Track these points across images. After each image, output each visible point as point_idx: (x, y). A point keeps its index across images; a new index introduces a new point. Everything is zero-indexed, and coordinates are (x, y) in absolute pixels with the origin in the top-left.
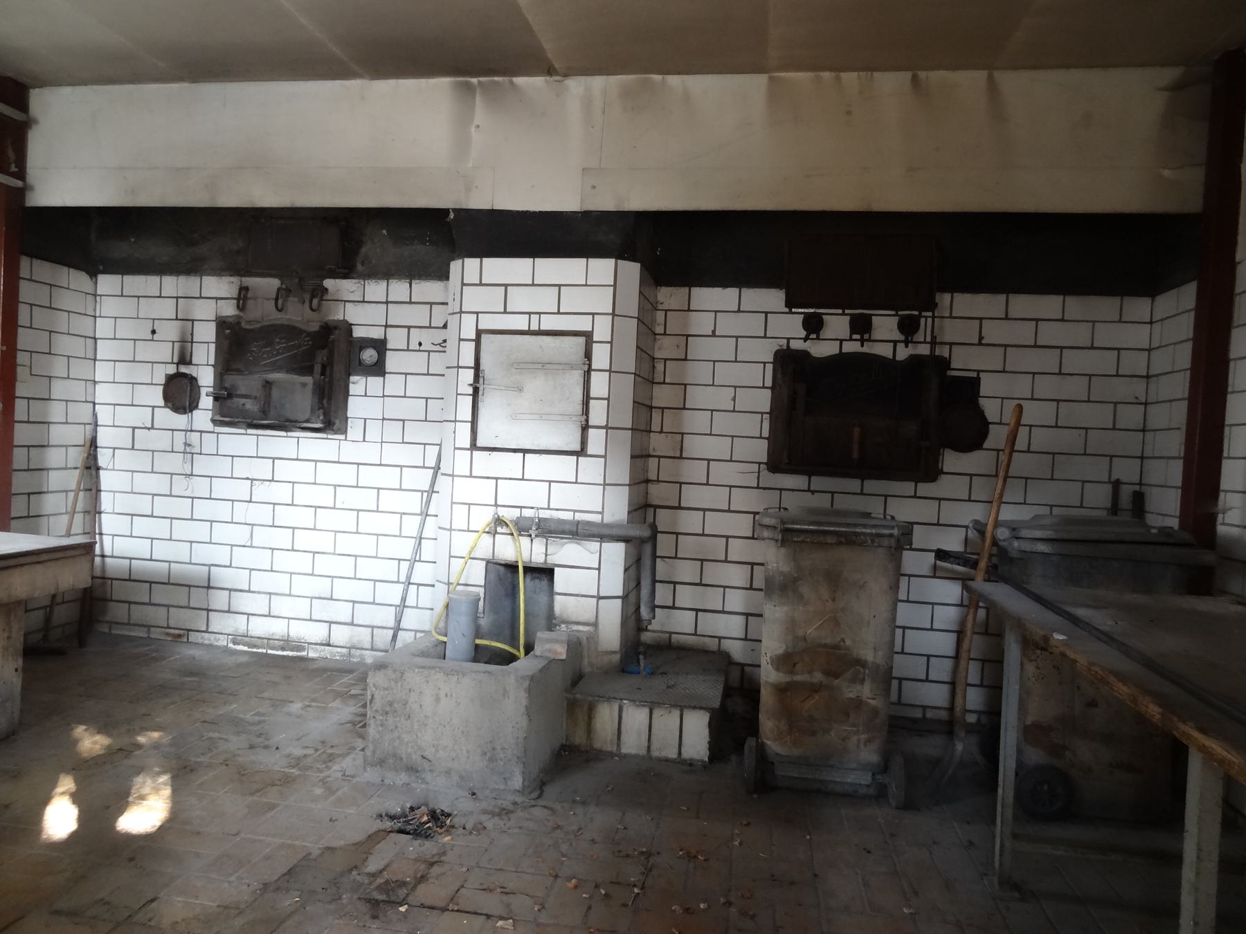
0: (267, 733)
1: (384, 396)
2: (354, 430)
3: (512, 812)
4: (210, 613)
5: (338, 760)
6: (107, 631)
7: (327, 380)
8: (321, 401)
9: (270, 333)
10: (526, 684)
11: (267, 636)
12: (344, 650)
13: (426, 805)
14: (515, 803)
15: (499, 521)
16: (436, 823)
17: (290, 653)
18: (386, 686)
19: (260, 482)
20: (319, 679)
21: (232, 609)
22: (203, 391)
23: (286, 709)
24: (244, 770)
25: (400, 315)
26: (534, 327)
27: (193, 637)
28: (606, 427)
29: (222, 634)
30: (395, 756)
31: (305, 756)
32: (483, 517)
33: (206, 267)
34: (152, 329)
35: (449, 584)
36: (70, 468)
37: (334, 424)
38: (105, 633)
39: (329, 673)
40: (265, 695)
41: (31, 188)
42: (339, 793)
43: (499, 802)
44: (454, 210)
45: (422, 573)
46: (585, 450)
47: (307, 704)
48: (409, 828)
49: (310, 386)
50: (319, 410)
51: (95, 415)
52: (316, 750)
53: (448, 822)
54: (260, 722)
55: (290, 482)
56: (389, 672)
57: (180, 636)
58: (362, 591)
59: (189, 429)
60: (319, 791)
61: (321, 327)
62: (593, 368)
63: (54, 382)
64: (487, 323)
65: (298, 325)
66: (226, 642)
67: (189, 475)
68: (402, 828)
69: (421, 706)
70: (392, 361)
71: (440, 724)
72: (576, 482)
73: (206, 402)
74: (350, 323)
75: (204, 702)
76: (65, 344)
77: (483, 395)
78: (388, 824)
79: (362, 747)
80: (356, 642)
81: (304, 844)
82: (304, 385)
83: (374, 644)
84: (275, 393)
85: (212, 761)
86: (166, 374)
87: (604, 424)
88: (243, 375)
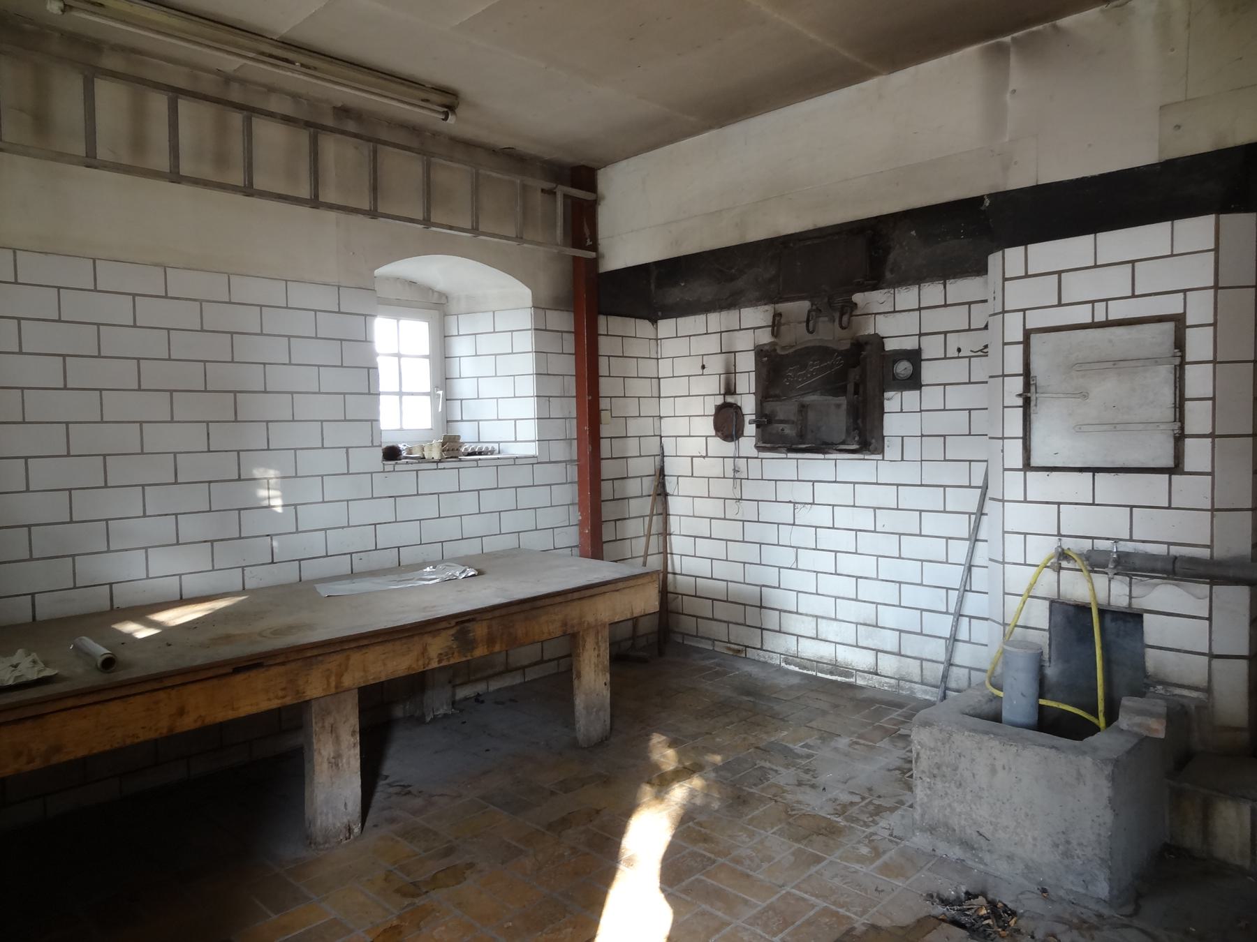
0: (815, 770)
1: (921, 411)
2: (891, 450)
3: (1097, 928)
4: (764, 632)
5: (884, 814)
6: (681, 641)
7: (860, 398)
8: (856, 418)
9: (803, 355)
10: (1108, 770)
11: (815, 659)
12: (893, 681)
13: (984, 895)
14: (1100, 916)
15: (1063, 555)
16: (997, 921)
17: (839, 679)
18: (932, 746)
19: (802, 506)
20: (867, 711)
21: (783, 630)
22: (747, 419)
23: (833, 744)
24: (792, 810)
25: (934, 321)
26: (1100, 317)
27: (751, 654)
28: (1212, 436)
29: (775, 653)
30: (946, 825)
31: (852, 804)
32: (1042, 549)
33: (743, 299)
34: (701, 364)
35: (1004, 625)
36: (645, 496)
37: (870, 444)
38: (679, 643)
39: (878, 705)
40: (814, 724)
41: (603, 256)
42: (885, 858)
43: (1079, 910)
44: (990, 196)
45: (973, 604)
46: (1180, 466)
47: (855, 740)
48: (964, 919)
49: (844, 407)
50: (854, 430)
51: (662, 447)
52: (863, 798)
53: (1012, 923)
54: (809, 756)
55: (830, 505)
56: (935, 730)
57: (739, 651)
58: (909, 620)
59: (737, 456)
60: (864, 850)
61: (852, 344)
62: (1187, 360)
63: (630, 421)
64: (1035, 320)
65: (830, 345)
66: (779, 661)
67: (739, 499)
68: (957, 917)
69: (974, 775)
70: (929, 373)
71: (998, 800)
72: (1169, 508)
73: (750, 429)
74: (881, 336)
75: (758, 725)
76: (640, 387)
77: (1036, 405)
78: (939, 910)
79: (910, 803)
80: (904, 673)
81: (848, 914)
82: (838, 406)
83: (924, 677)
84: (811, 416)
85: (763, 794)
86: (716, 405)
87: (1208, 430)
88: (781, 401)
